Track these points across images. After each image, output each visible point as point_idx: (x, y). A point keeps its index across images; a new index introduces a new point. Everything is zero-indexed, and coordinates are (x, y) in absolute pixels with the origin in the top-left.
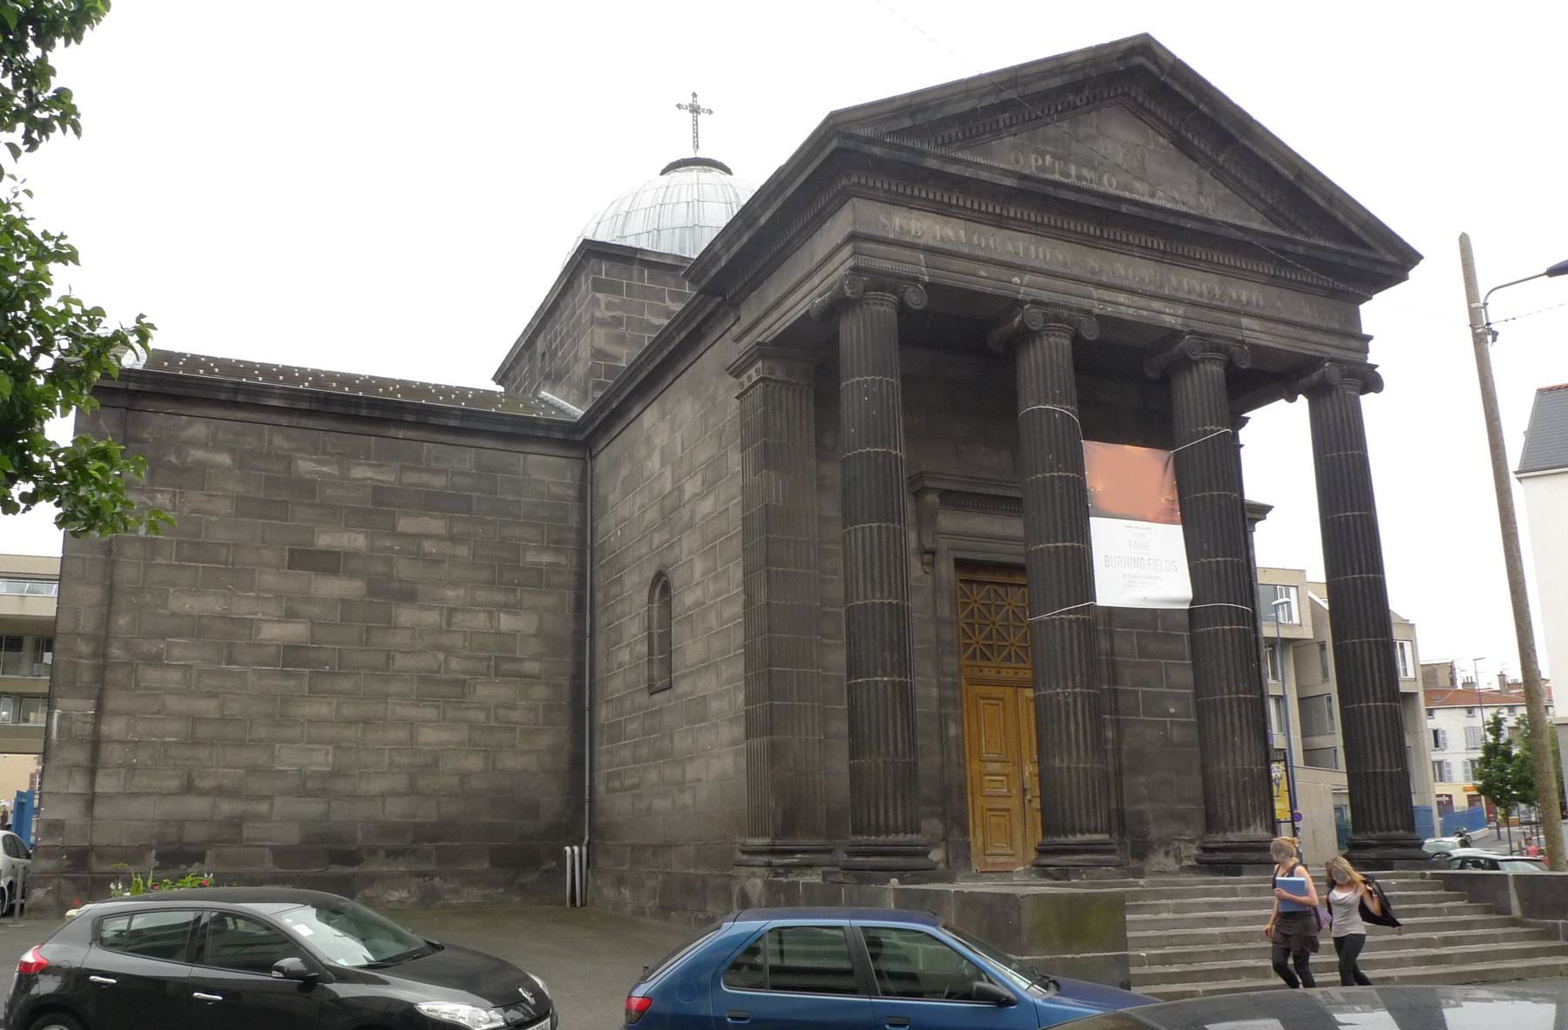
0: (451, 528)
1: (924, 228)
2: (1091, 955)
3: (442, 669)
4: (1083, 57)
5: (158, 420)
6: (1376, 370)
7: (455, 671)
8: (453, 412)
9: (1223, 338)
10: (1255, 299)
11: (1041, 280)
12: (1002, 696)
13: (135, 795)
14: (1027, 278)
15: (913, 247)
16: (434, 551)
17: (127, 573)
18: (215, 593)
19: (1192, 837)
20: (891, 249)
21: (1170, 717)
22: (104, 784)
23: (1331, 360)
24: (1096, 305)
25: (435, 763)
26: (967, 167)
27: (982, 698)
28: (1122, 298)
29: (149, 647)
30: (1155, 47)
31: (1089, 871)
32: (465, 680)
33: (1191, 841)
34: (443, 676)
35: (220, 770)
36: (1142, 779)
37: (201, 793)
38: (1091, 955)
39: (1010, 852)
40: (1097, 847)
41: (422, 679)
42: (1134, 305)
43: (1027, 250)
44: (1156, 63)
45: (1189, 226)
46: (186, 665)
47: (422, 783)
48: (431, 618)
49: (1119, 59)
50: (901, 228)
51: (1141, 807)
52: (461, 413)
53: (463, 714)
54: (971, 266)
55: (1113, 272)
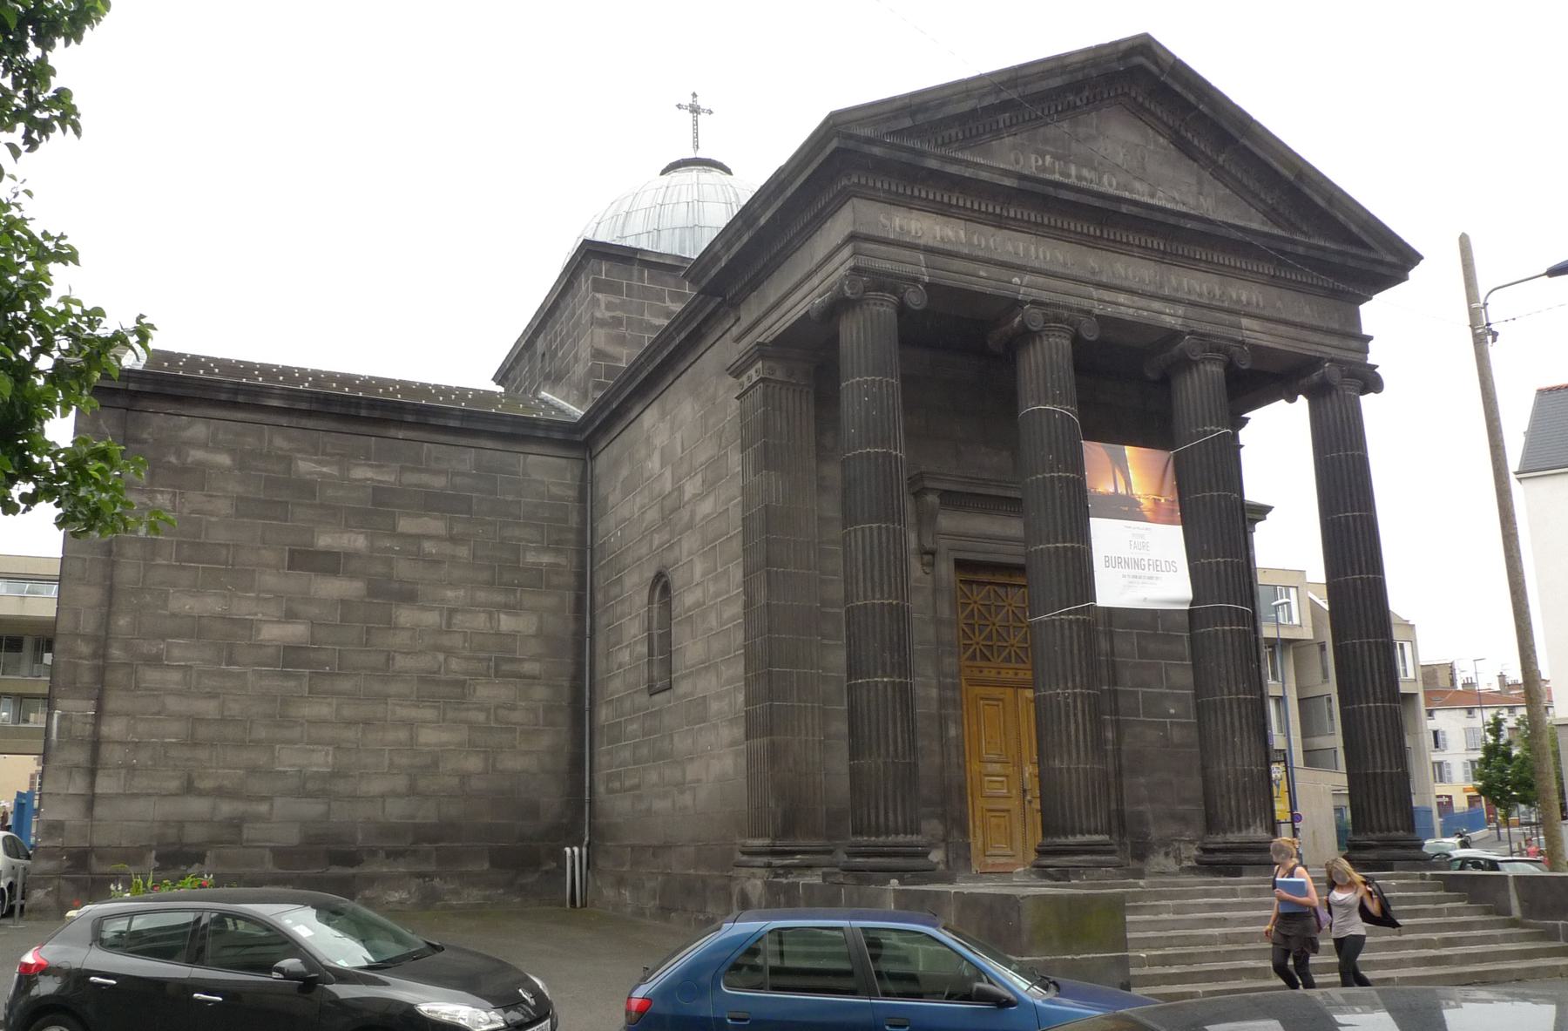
0: (451, 528)
2: (1091, 956)
3: (442, 670)
4: (1083, 57)
5: (158, 421)
6: (1376, 370)
8: (453, 413)
9: (1223, 338)
10: (1255, 300)
11: (1041, 280)
12: (1002, 696)
13: (135, 796)
14: (1027, 278)
15: (913, 247)
17: (127, 574)
18: (215, 594)
22: (104, 785)
23: (1331, 360)
25: (436, 764)
26: (967, 167)
27: (982, 699)
28: (1122, 298)
29: (148, 648)
30: (1155, 47)
31: (1089, 872)
32: (465, 680)
33: (1191, 842)
34: (443, 677)
35: (219, 771)
36: (1142, 780)
37: (201, 793)
38: (1091, 956)
39: (1010, 853)
40: (1097, 848)
41: (422, 680)
42: (1134, 305)
43: (1027, 250)
44: (1156, 63)
45: (1189, 226)
46: (186, 666)
47: (422, 783)
48: (431, 618)
49: (1119, 59)
50: (901, 228)
51: (1141, 808)
53: (463, 715)
54: (971, 266)
55: (1113, 273)
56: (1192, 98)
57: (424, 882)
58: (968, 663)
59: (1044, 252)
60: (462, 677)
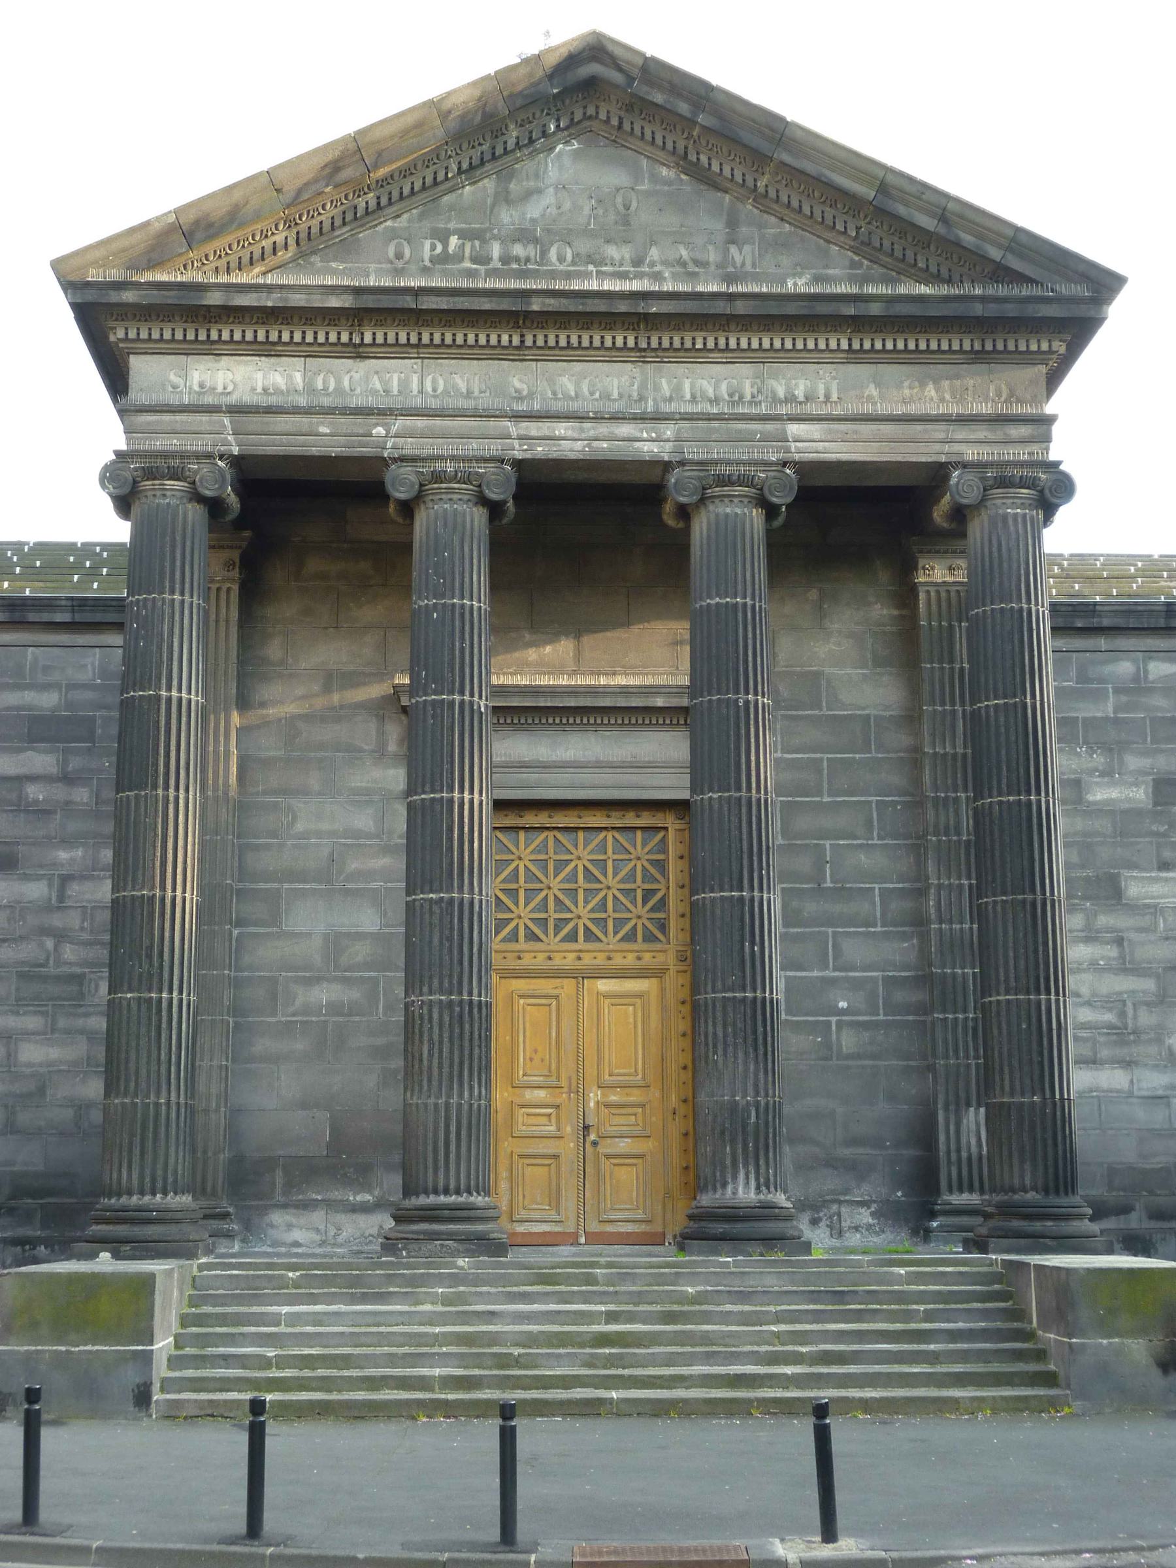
0: (65, 762)
1: (238, 378)
3: (51, 962)
6: (1061, 467)
7: (70, 963)
8: (58, 603)
11: (420, 423)
12: (555, 992)
14: (398, 424)
16: (41, 798)
19: (866, 1198)
20: (179, 418)
21: (838, 1015)
24: (517, 447)
25: (41, 1091)
27: (521, 997)
28: (561, 428)
30: (610, 47)
31: (413, 1246)
32: (85, 974)
33: (862, 1204)
34: (52, 970)
38: (97, 1348)
39: (557, 1218)
41: (22, 976)
42: (583, 436)
43: (404, 385)
44: (620, 69)
47: (24, 1118)
48: (36, 891)
52: (69, 603)
53: (80, 1022)
54: (304, 421)
55: (554, 393)
56: (684, 108)
57: (24, 1251)
58: (504, 946)
59: (434, 381)
60: (78, 970)
